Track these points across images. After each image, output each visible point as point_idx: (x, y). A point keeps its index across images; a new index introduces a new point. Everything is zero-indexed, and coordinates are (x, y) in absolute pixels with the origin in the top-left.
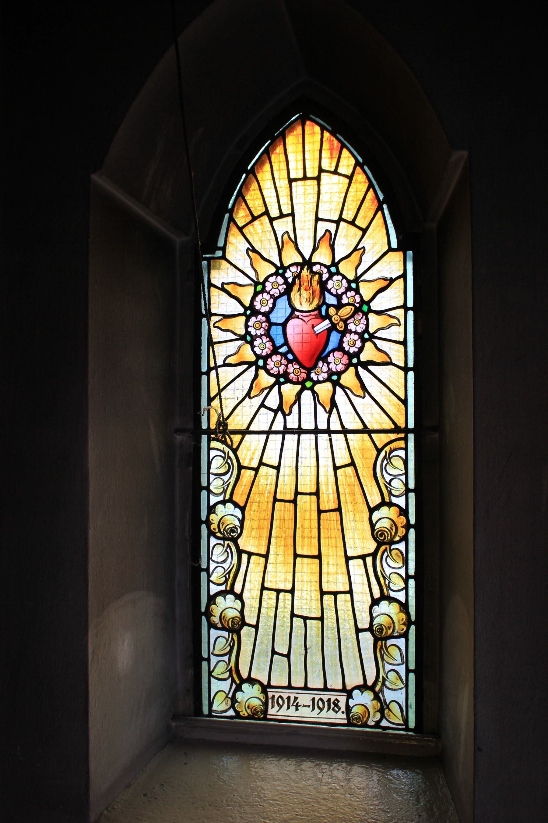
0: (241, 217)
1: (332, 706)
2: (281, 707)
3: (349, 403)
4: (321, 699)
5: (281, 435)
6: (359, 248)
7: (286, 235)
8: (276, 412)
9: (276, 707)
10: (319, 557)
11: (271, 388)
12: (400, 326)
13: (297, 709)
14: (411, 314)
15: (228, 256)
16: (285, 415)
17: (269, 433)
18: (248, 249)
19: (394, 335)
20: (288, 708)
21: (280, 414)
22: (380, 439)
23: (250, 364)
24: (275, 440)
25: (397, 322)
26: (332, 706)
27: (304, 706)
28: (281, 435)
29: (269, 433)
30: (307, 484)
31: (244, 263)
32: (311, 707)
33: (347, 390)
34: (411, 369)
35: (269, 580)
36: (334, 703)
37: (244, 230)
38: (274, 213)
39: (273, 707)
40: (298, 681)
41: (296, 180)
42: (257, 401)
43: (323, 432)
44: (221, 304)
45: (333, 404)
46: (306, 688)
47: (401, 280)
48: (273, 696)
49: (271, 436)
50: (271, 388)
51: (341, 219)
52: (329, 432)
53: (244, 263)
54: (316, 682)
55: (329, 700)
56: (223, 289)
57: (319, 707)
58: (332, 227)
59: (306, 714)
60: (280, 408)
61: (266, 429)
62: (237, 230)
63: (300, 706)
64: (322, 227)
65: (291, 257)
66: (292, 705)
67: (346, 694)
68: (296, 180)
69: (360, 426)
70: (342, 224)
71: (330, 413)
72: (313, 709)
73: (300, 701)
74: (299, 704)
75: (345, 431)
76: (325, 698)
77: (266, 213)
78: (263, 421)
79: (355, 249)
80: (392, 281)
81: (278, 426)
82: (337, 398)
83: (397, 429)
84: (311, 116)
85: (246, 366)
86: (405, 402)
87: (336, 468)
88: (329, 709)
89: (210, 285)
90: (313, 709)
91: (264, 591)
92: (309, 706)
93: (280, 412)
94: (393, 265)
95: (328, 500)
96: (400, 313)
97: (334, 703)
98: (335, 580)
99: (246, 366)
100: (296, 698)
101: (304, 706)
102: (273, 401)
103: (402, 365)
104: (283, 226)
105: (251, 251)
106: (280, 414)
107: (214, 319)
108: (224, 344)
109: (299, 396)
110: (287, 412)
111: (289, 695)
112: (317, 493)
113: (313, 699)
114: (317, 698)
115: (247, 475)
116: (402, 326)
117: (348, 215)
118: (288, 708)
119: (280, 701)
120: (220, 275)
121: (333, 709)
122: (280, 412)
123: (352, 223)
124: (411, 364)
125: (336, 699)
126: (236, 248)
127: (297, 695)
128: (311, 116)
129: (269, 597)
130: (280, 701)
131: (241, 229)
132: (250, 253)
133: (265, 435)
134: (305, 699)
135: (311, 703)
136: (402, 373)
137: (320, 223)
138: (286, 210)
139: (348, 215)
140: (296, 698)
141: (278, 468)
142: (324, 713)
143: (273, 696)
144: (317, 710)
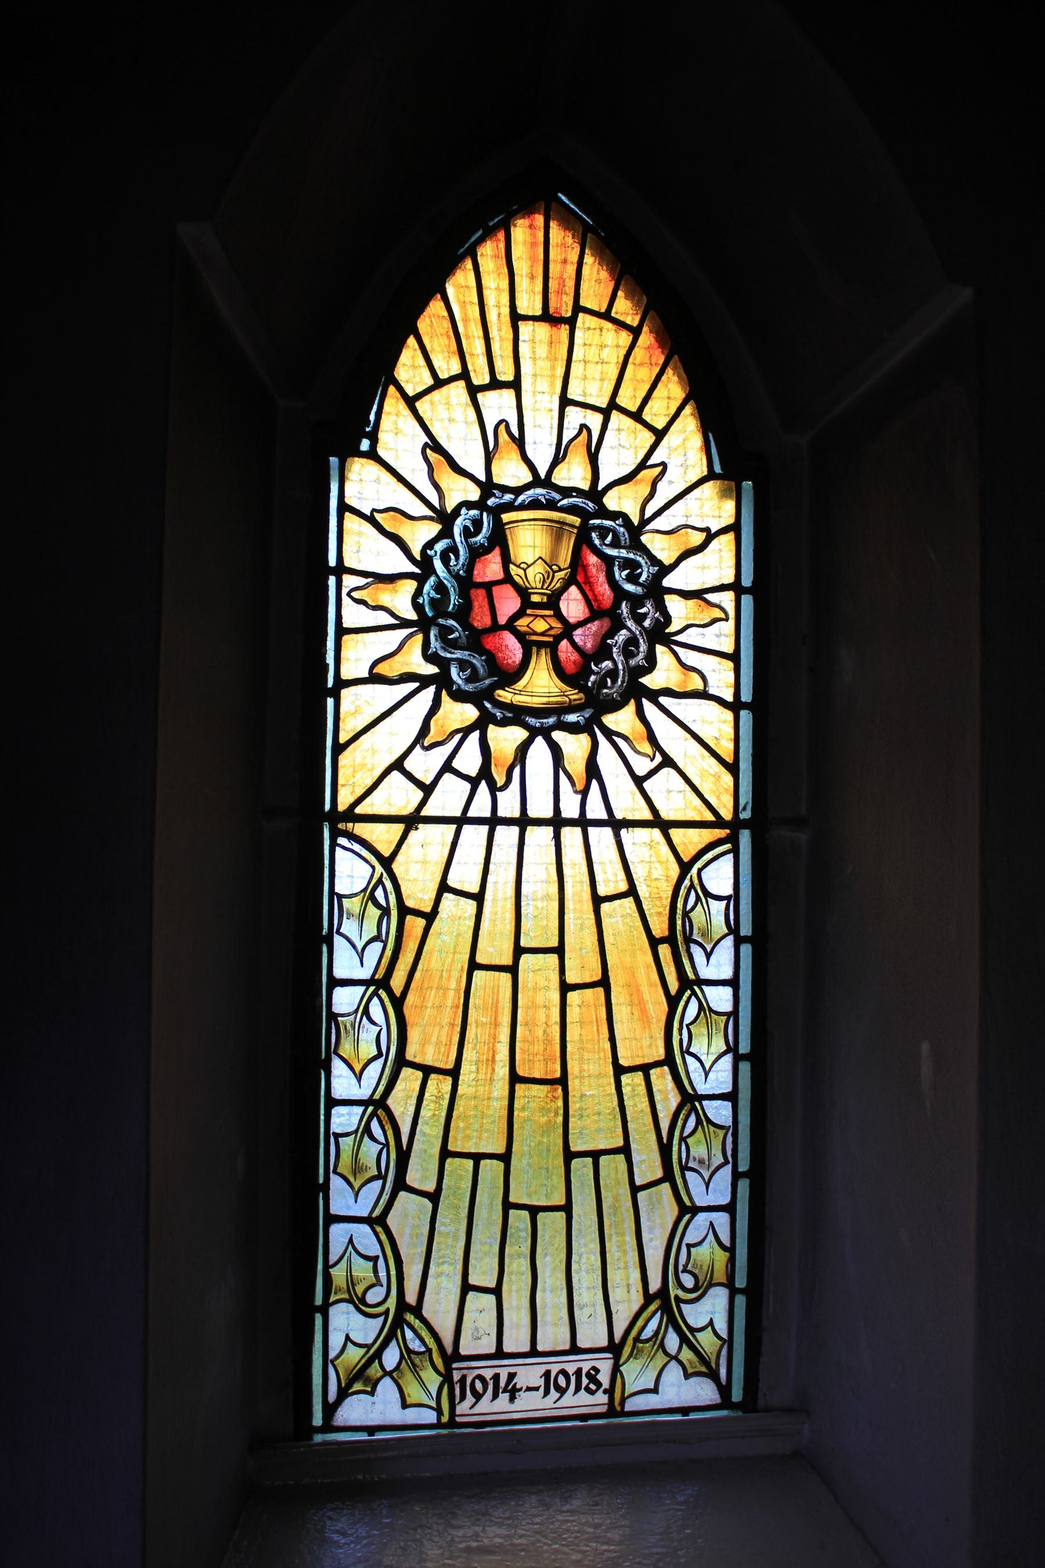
0: (410, 370)
1: (585, 1381)
2: (478, 1397)
3: (443, 1120)
4: (563, 1372)
5: (487, 827)
6: (650, 463)
7: (502, 427)
8: (474, 782)
9: (470, 1399)
10: (563, 1081)
11: (466, 731)
12: (727, 620)
13: (512, 1399)
14: (747, 600)
15: (381, 452)
16: (493, 789)
17: (461, 821)
18: (426, 445)
19: (707, 649)
20: (495, 1396)
21: (483, 786)
22: (689, 841)
23: (424, 681)
24: (474, 836)
25: (723, 616)
26: (585, 1381)
27: (529, 1389)
28: (487, 827)
29: (461, 821)
30: (539, 930)
31: (417, 474)
32: (542, 1389)
33: (620, 741)
34: (746, 706)
35: (547, 1286)
36: (588, 1375)
37: (418, 405)
38: (481, 378)
39: (463, 1397)
40: (516, 1340)
41: (526, 318)
42: (440, 754)
43: (571, 822)
44: (362, 548)
45: (593, 770)
46: (534, 1352)
47: (730, 537)
48: (463, 1378)
49: (467, 829)
50: (466, 731)
51: (613, 405)
52: (583, 822)
53: (417, 474)
54: (553, 1334)
55: (578, 1372)
56: (371, 520)
57: (558, 1388)
58: (595, 421)
59: (530, 1404)
60: (485, 772)
61: (458, 813)
62: (402, 406)
63: (521, 1389)
64: (575, 417)
65: (510, 472)
66: (505, 1391)
67: (611, 1356)
68: (526, 318)
69: (647, 815)
70: (615, 416)
71: (585, 793)
72: (547, 1392)
73: (520, 1381)
74: (518, 1386)
75: (616, 825)
76: (571, 1369)
77: (464, 375)
78: (449, 798)
79: (642, 466)
80: (710, 536)
81: (481, 807)
82: (601, 760)
83: (719, 822)
84: (560, 195)
85: (415, 685)
86: (733, 768)
87: (598, 901)
88: (578, 1389)
89: (344, 508)
90: (547, 1392)
91: (445, 895)
92: (537, 1389)
93: (483, 782)
94: (713, 507)
95: (582, 965)
96: (727, 599)
97: (588, 1375)
98: (594, 1129)
99: (415, 685)
100: (512, 1376)
101: (529, 1389)
102: (469, 760)
103: (730, 698)
104: (498, 405)
105: (432, 449)
106: (483, 786)
107: (350, 581)
108: (370, 637)
109: (523, 750)
110: (500, 783)
111: (497, 1370)
112: (559, 950)
113: (547, 1374)
114: (555, 1369)
115: (415, 925)
116: (732, 622)
117: (628, 399)
118: (495, 1396)
119: (479, 1385)
120: (363, 484)
121: (588, 1390)
122: (483, 782)
123: (637, 416)
124: (746, 696)
125: (594, 1368)
126: (397, 434)
127: (512, 1370)
128: (560, 195)
129: (459, 1170)
130: (479, 1385)
131: (411, 402)
132: (428, 451)
133: (454, 827)
134: (530, 1375)
135: (541, 1382)
136: (729, 715)
137: (570, 410)
138: (506, 373)
139: (628, 399)
140: (512, 1376)
141: (479, 898)
142: (568, 1400)
143: (463, 1378)
144: (554, 1394)
